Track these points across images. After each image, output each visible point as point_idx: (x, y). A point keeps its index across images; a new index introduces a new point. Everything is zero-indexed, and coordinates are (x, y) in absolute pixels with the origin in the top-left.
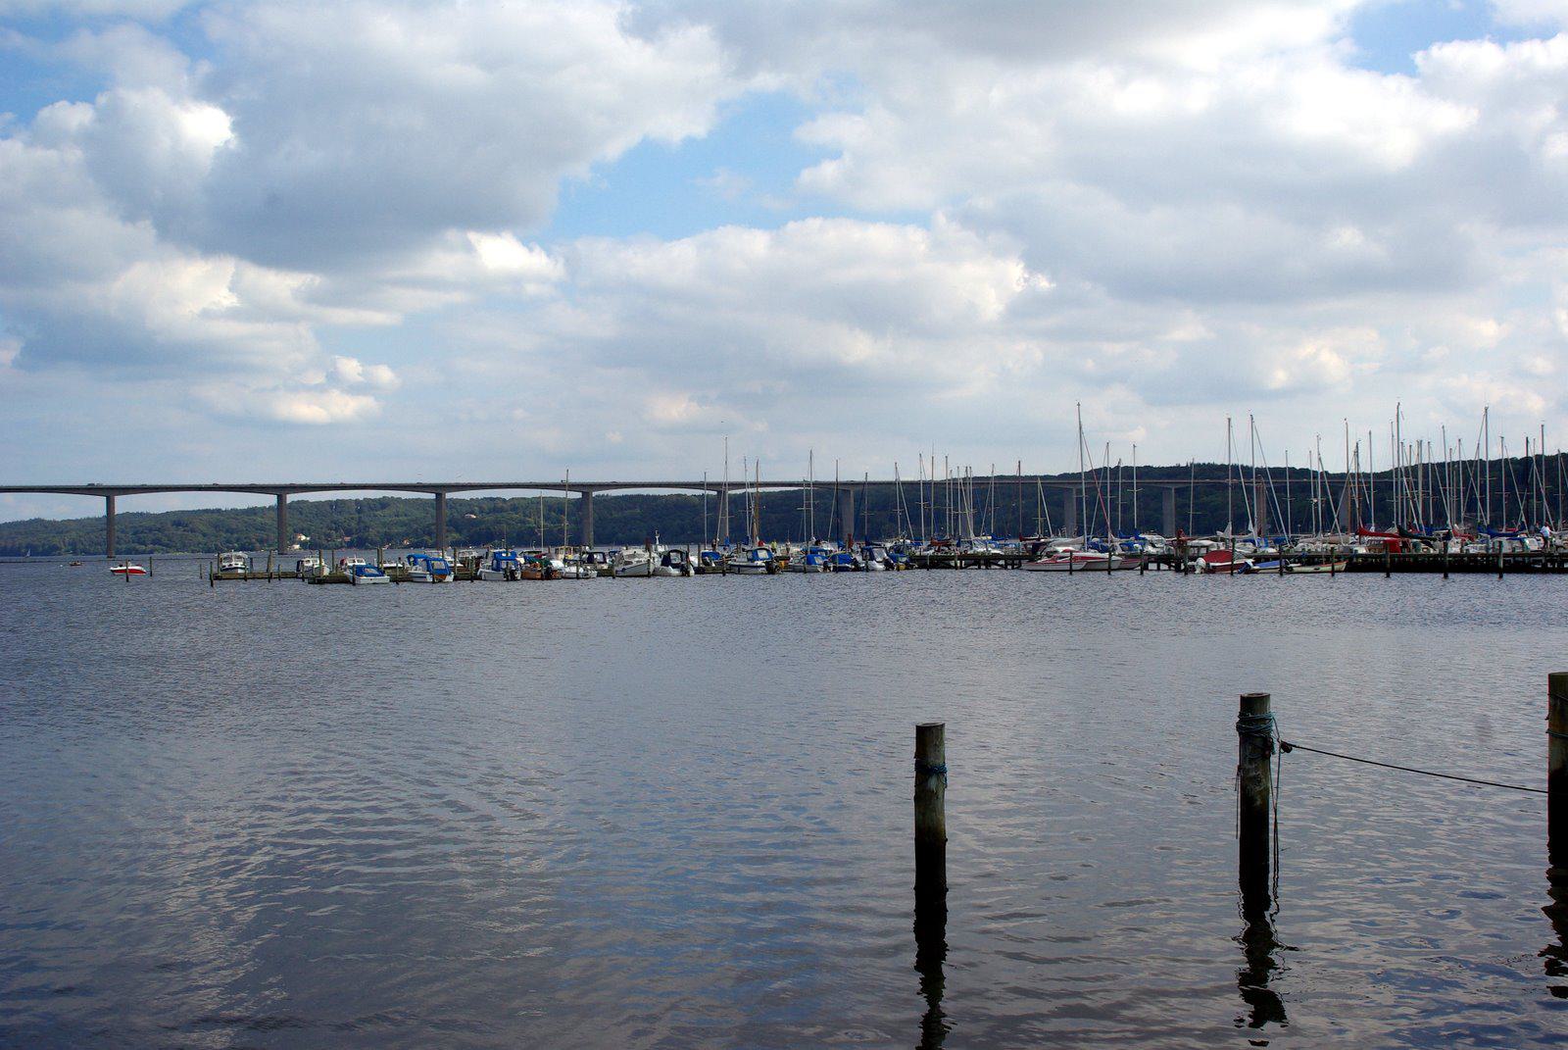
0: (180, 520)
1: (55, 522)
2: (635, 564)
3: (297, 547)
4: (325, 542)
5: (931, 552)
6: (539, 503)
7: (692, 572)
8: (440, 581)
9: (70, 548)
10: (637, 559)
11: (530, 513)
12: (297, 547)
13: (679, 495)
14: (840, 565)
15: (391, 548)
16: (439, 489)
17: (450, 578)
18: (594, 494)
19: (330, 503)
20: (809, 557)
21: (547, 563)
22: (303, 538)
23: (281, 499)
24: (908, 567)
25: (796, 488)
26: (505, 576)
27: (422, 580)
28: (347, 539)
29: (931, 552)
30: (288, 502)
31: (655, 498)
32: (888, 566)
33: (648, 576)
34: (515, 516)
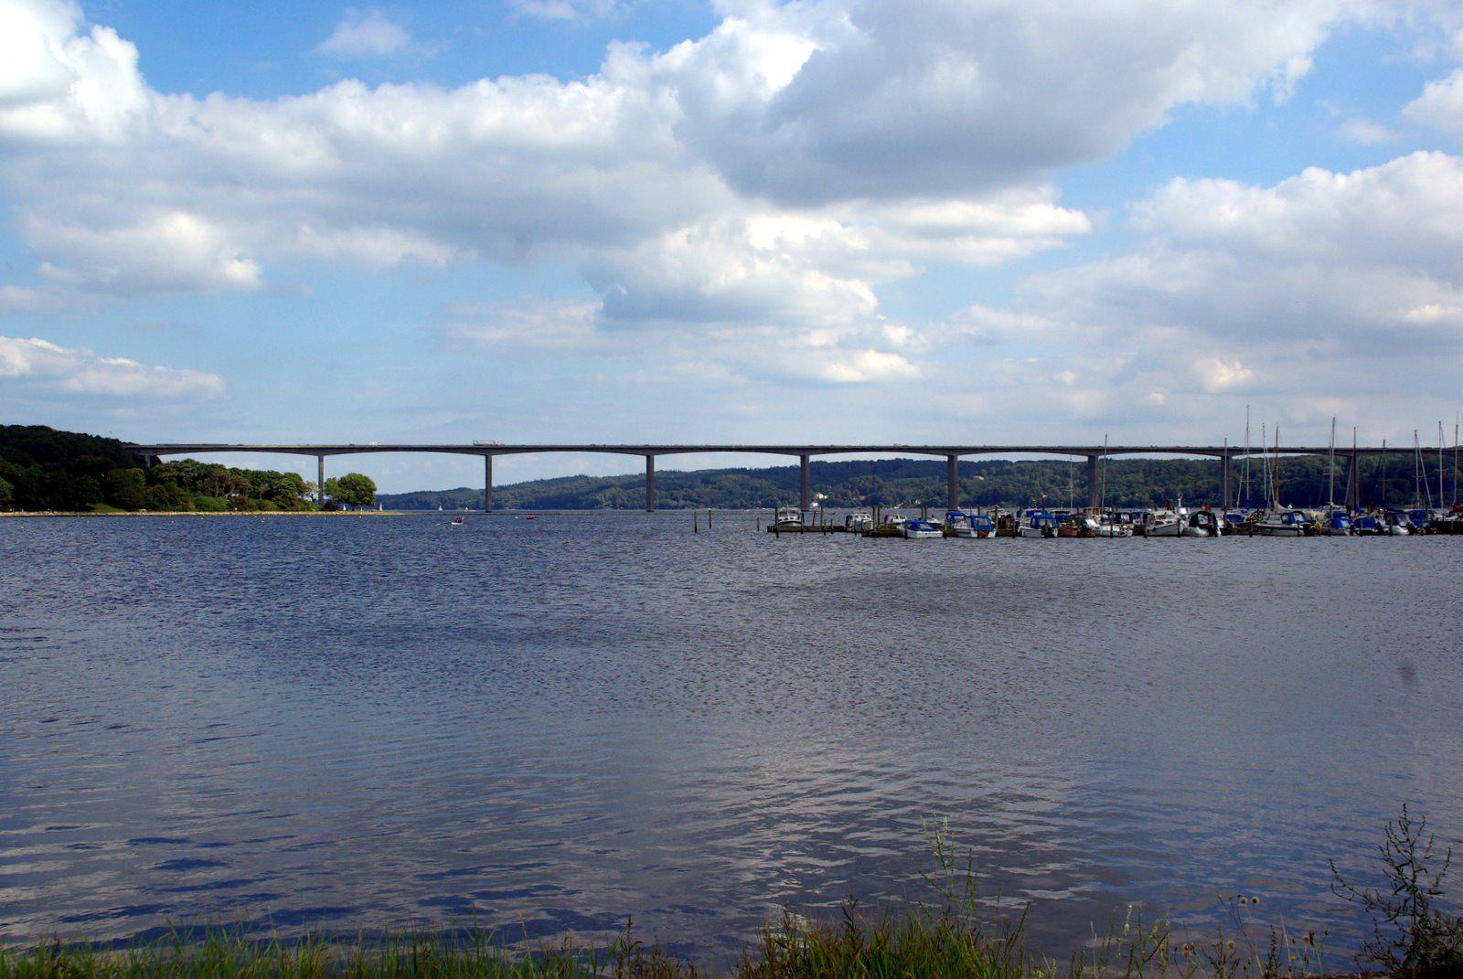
0: (707, 477)
1: (597, 478)
2: (1165, 524)
3: (815, 504)
4: (841, 501)
5: (1454, 518)
6: (1454, 451)
7: (1219, 533)
8: (984, 537)
9: (610, 502)
10: (1167, 520)
11: (1036, 475)
12: (815, 504)
13: (1181, 460)
14: (1365, 528)
15: (902, 507)
16: (951, 451)
17: (992, 534)
18: (1235, 458)
19: (846, 464)
20: (1334, 521)
21: (1083, 522)
22: (821, 496)
23: (804, 459)
24: (1429, 532)
25: (1208, 457)
26: (1043, 533)
27: (966, 535)
28: (863, 498)
29: (1454, 518)
30: (810, 461)
31: (1158, 463)
32: (1412, 531)
33: (1179, 535)
34: (1021, 478)
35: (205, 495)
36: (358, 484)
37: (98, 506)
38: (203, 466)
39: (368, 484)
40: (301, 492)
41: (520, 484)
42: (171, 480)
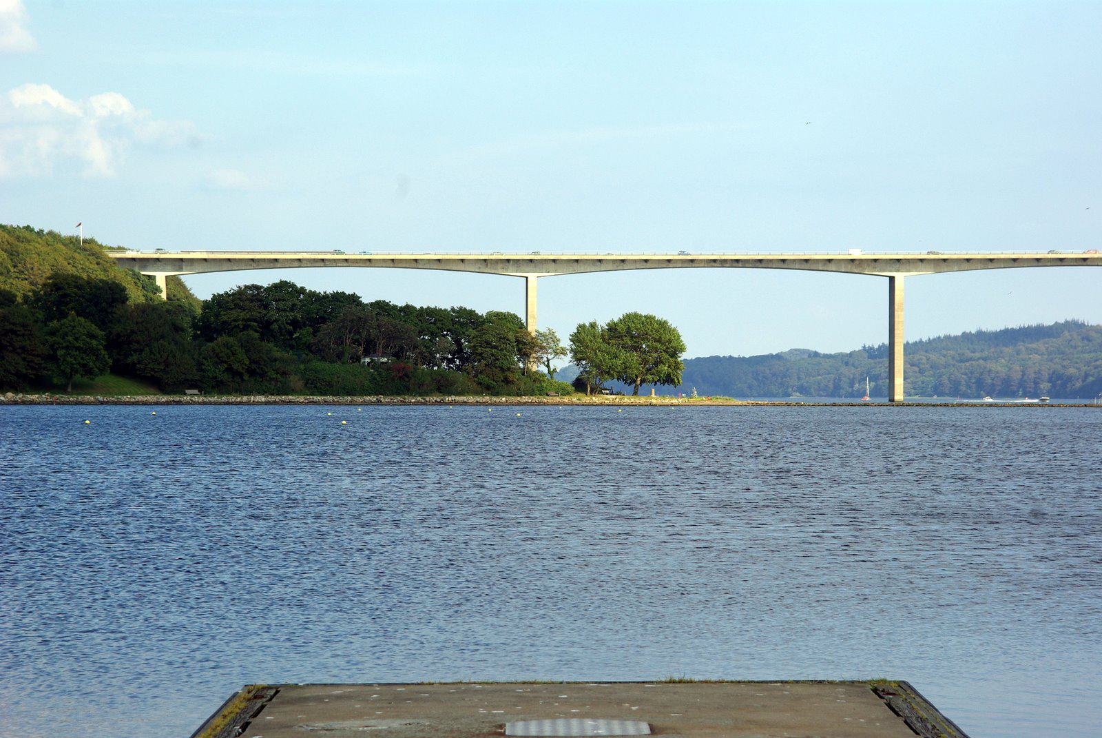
35: (323, 359)
36: (644, 336)
37: (99, 380)
38: (313, 296)
39: (666, 337)
40: (525, 356)
41: (930, 342)
42: (246, 327)
